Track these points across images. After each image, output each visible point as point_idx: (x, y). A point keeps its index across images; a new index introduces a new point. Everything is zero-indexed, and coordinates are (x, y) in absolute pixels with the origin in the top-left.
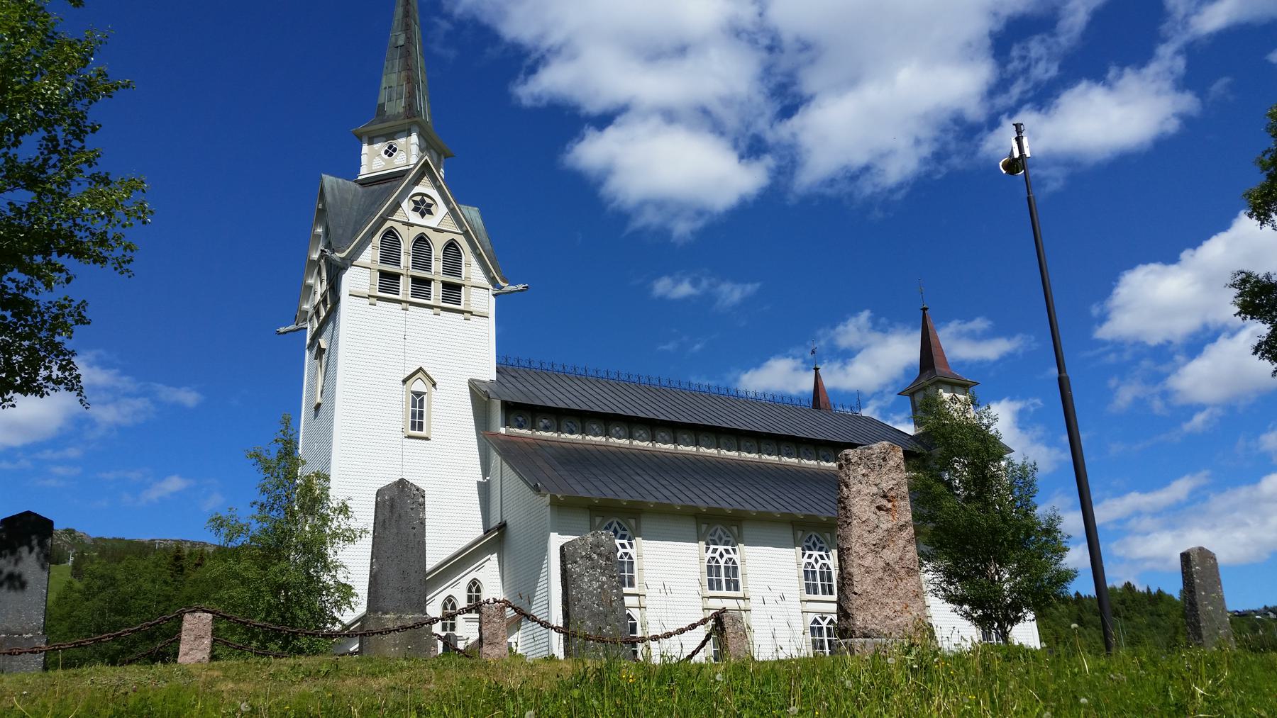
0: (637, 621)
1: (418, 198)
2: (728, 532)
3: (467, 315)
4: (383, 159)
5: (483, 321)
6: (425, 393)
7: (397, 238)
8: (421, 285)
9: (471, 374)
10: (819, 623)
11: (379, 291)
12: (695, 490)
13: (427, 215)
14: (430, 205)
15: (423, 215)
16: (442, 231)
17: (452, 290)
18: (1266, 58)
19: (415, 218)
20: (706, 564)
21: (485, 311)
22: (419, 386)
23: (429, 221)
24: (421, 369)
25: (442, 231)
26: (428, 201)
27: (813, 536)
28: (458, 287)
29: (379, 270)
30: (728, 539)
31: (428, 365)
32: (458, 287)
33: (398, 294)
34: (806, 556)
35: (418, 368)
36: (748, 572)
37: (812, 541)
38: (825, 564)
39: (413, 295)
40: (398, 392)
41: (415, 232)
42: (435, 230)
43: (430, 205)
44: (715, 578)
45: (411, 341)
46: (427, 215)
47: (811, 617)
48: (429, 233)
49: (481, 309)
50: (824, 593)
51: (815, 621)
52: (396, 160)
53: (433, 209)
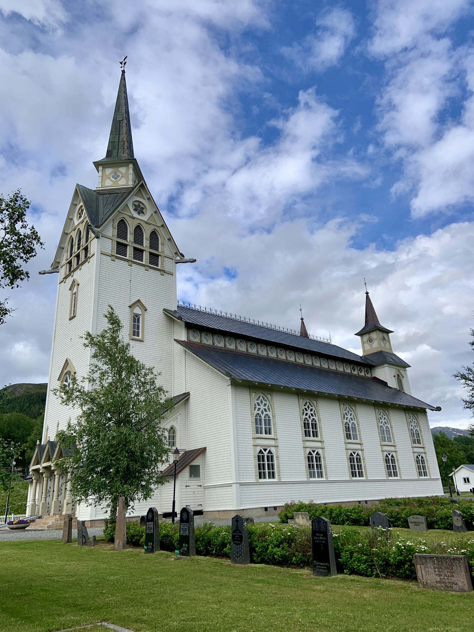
0: (274, 455)
1: (137, 204)
2: (266, 398)
3: (162, 273)
4: (112, 181)
5: (170, 277)
6: (140, 315)
7: (126, 225)
8: (138, 253)
9: (164, 306)
10: (263, 453)
11: (116, 254)
12: (271, 378)
13: (141, 214)
14: (143, 208)
15: (139, 214)
16: (149, 224)
17: (154, 258)
18: (461, 104)
19: (135, 215)
20: (254, 417)
21: (171, 271)
22: (137, 310)
23: (145, 218)
24: (139, 300)
25: (149, 224)
26: (142, 206)
27: (308, 402)
28: (157, 256)
29: (149, 252)
30: (266, 402)
31: (143, 299)
32: (157, 256)
33: (126, 257)
34: (257, 409)
35: (137, 300)
36: (277, 423)
37: (307, 406)
38: (267, 415)
39: (134, 258)
40: (127, 313)
41: (135, 223)
42: (146, 223)
43: (143, 208)
44: (259, 426)
45: (133, 284)
46: (141, 214)
47: (258, 449)
48: (143, 224)
49: (169, 270)
50: (266, 433)
51: (261, 452)
52: (120, 182)
53: (144, 211)
